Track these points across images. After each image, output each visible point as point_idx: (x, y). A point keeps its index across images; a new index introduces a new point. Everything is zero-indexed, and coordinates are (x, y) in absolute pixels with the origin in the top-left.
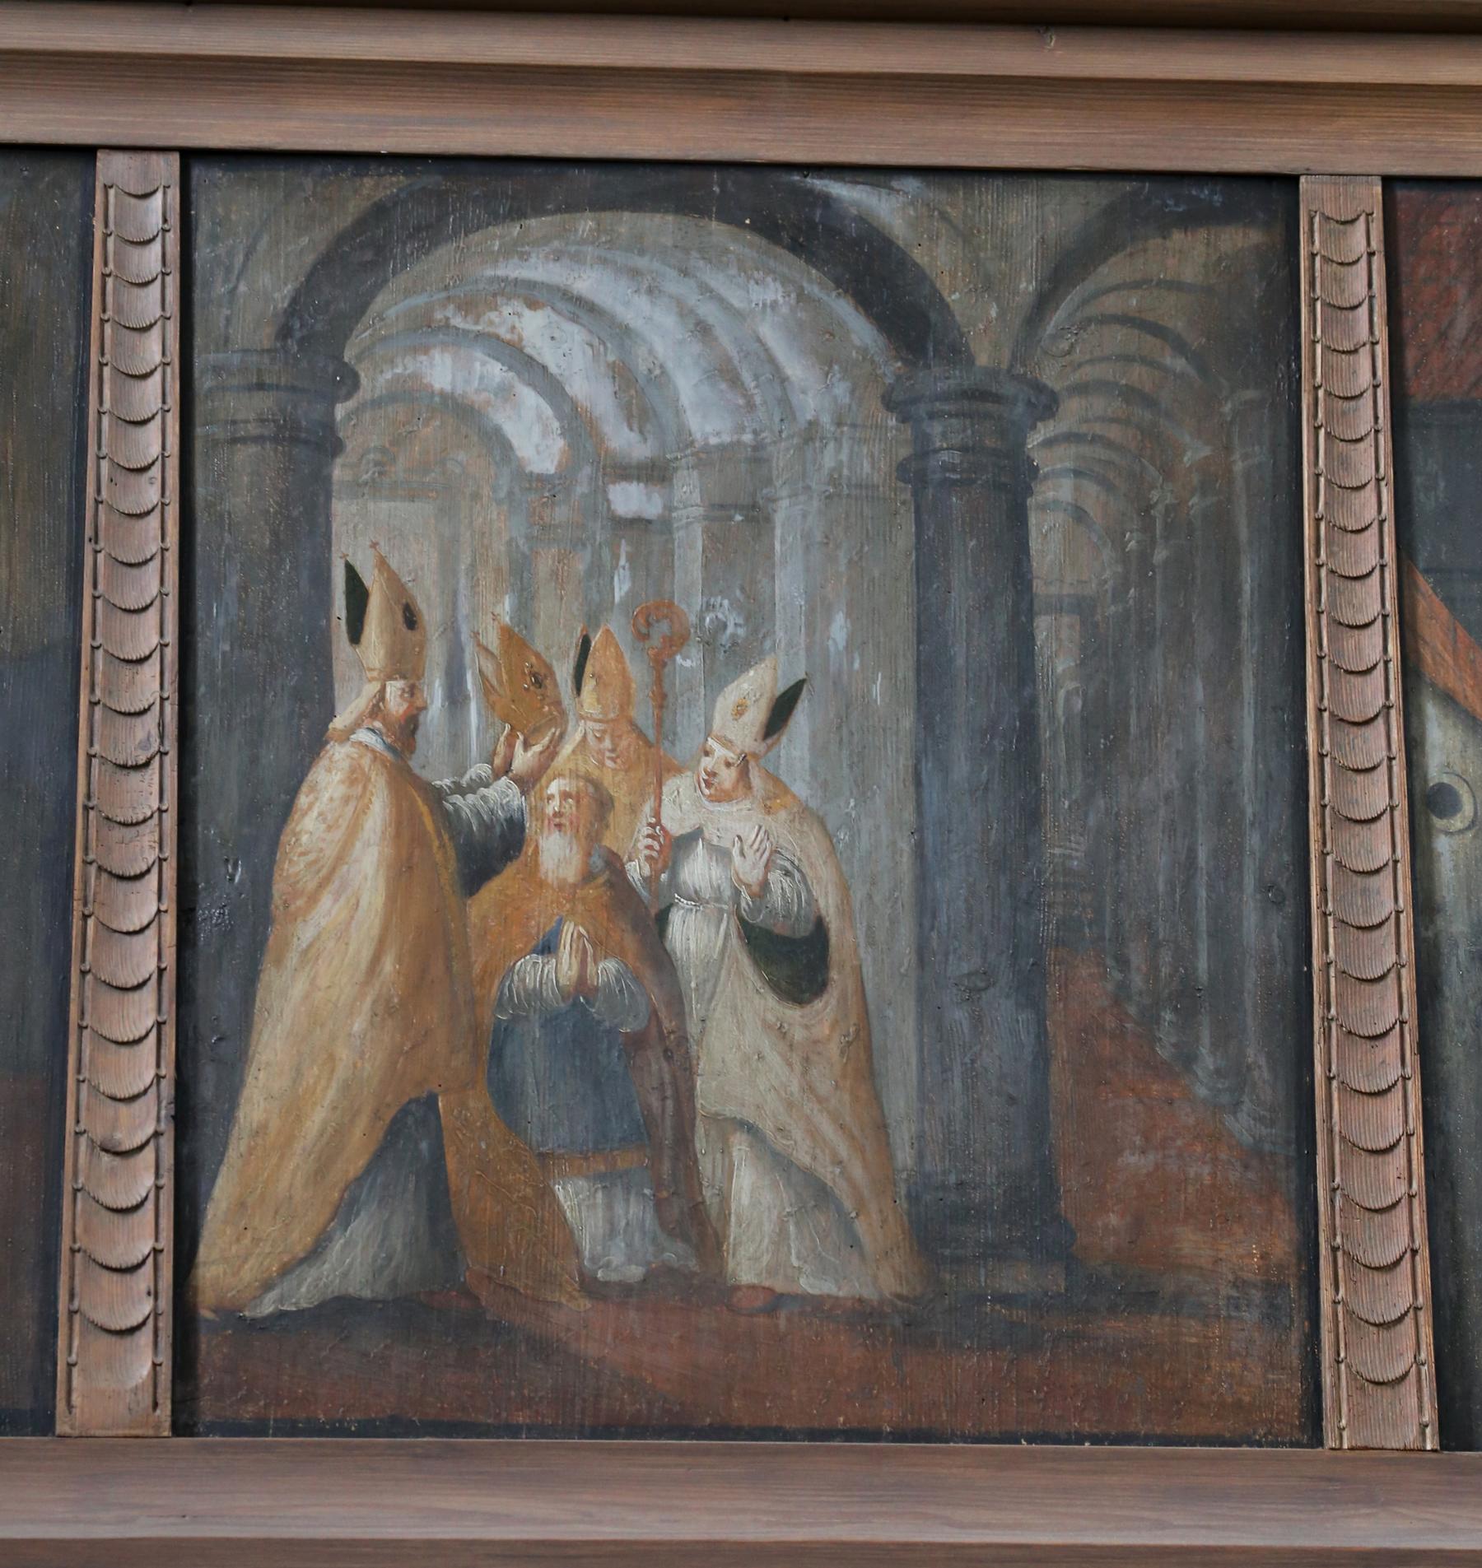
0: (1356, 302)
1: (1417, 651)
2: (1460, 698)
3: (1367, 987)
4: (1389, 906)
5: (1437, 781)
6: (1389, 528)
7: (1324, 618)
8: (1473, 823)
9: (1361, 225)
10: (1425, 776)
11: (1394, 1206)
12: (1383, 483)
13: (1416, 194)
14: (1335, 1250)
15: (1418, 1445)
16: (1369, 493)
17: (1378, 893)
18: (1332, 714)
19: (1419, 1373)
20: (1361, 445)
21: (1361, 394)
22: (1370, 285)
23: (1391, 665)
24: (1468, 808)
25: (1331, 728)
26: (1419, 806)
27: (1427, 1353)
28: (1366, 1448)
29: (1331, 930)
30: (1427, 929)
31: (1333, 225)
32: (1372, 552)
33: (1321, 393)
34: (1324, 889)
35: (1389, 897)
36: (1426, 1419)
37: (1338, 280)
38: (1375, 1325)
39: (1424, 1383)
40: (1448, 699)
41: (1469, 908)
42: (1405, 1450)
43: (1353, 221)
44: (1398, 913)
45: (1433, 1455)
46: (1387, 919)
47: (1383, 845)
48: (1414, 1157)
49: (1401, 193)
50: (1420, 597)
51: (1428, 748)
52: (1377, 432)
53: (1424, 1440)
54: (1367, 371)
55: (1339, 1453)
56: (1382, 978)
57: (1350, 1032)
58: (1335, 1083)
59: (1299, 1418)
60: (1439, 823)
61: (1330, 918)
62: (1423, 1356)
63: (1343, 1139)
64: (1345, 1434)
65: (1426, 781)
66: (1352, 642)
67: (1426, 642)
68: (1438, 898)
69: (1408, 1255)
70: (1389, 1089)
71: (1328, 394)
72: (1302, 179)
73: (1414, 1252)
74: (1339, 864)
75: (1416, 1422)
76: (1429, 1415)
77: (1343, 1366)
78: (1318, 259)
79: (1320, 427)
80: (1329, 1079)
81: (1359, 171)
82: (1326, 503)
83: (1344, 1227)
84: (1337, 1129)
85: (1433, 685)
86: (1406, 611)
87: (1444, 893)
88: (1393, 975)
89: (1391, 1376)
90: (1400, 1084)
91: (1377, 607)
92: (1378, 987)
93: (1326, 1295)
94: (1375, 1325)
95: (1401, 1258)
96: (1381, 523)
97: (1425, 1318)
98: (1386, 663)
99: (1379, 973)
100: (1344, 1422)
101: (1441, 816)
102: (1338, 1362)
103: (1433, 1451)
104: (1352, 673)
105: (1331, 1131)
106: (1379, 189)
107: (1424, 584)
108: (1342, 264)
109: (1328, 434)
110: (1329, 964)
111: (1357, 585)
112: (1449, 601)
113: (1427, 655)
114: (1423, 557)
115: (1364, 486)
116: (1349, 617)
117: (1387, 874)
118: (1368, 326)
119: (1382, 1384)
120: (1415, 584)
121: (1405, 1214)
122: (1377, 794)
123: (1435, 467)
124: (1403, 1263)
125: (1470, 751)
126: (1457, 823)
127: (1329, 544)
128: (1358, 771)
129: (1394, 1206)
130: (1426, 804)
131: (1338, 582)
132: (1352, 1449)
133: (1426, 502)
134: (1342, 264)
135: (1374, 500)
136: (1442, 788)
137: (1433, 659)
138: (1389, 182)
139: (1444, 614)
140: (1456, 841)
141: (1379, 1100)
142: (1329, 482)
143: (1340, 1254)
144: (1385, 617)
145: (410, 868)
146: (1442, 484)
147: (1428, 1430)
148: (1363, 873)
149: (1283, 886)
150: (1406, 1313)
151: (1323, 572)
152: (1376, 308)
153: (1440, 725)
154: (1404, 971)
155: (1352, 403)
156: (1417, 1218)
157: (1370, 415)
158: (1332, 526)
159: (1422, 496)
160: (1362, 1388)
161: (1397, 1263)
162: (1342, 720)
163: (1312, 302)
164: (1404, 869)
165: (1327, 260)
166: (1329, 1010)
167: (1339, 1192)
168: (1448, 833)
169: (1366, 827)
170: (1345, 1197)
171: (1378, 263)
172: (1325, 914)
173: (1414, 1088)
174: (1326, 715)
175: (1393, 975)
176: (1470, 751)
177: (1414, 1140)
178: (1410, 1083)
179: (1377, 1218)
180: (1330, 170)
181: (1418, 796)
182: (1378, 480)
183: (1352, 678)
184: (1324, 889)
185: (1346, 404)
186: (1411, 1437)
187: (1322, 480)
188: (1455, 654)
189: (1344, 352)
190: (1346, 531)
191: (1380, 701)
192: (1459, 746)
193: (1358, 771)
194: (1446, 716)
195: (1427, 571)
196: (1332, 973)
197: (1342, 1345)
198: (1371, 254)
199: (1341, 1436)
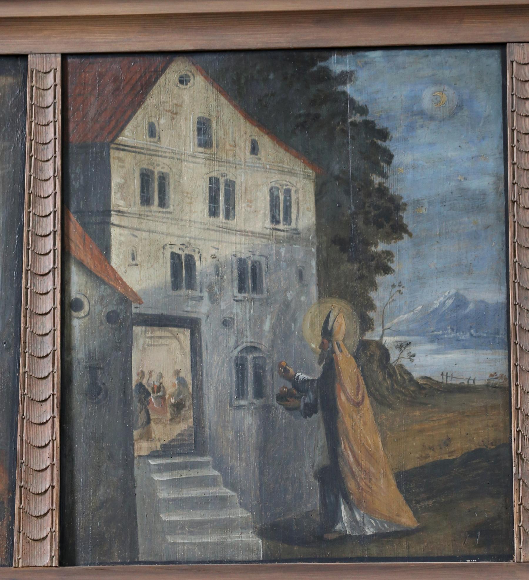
0: (49, 105)
1: (69, 245)
2: (85, 263)
3: (41, 381)
4: (51, 349)
5: (74, 297)
6: (59, 196)
7: (30, 233)
8: (88, 313)
9: (52, 73)
10: (70, 294)
11: (46, 469)
12: (57, 178)
13: (77, 60)
14: (21, 487)
15: (50, 564)
16: (51, 182)
17: (47, 343)
18: (32, 272)
19: (52, 536)
20: (49, 163)
21: (50, 142)
22: (55, 98)
23: (56, 251)
24: (86, 308)
25: (31, 277)
26: (67, 307)
27: (56, 528)
28: (35, 566)
29: (27, 359)
30: (67, 357)
31: (41, 74)
32: (49, 206)
33: (33, 142)
34: (25, 342)
35: (49, 345)
36: (53, 554)
37: (43, 96)
38: (35, 517)
39: (54, 540)
40: (81, 264)
41: (85, 349)
42: (44, 566)
43: (49, 72)
44: (54, 351)
45: (56, 569)
46: (50, 354)
47: (48, 324)
48: (55, 449)
49: (70, 60)
50: (71, 223)
51: (72, 284)
52: (55, 157)
53: (52, 563)
54: (51, 133)
55: (17, 569)
56: (47, 377)
57: (32, 399)
58: (25, 420)
59: (5, 555)
60: (75, 314)
61: (27, 354)
62: (54, 529)
63: (27, 442)
64: (20, 561)
65: (70, 297)
66: (42, 242)
67: (73, 241)
68: (73, 344)
69: (50, 489)
70: (47, 422)
71: (36, 142)
72: (29, 56)
73: (53, 487)
74: (31, 332)
75: (49, 555)
76: (55, 552)
77: (21, 534)
78: (34, 88)
79: (32, 156)
80: (23, 419)
81: (51, 52)
82: (33, 187)
83: (25, 478)
84: (24, 439)
85: (75, 258)
86: (65, 229)
87: (75, 342)
88: (51, 376)
89: (41, 537)
90: (51, 419)
91: (52, 228)
92: (44, 381)
93: (17, 506)
94: (35, 517)
95: (47, 490)
96: (55, 194)
97: (56, 514)
98: (55, 250)
99: (45, 375)
100: (20, 557)
101: (75, 311)
102: (19, 532)
103: (56, 567)
104: (41, 255)
105: (22, 439)
106: (59, 59)
107: (73, 218)
108: (44, 90)
109: (35, 159)
110: (25, 372)
111: (45, 219)
112: (84, 225)
113: (73, 246)
114: (73, 206)
115: (49, 179)
116: (40, 232)
117: (50, 336)
118: (52, 115)
119: (37, 540)
120: (69, 218)
121: (50, 472)
122: (47, 304)
123: (79, 171)
124: (48, 492)
125: (89, 285)
126: (82, 314)
127: (34, 204)
128: (41, 294)
129: (46, 469)
130: (67, 306)
131: (37, 218)
132: (22, 567)
133: (75, 184)
134: (44, 90)
135: (53, 185)
136: (77, 301)
137: (75, 248)
138: (65, 56)
139: (80, 229)
140: (81, 322)
141: (43, 426)
142: (34, 178)
143: (23, 489)
144: (55, 232)
145: (283, 171)
146: (82, 178)
147: (54, 559)
148: (41, 335)
149: (10, 341)
150: (48, 512)
151: (31, 214)
152: (57, 107)
153: (77, 274)
154: (55, 374)
155: (46, 146)
156: (55, 473)
157: (51, 152)
158: (35, 196)
159: (74, 183)
160: (29, 542)
161: (46, 491)
162: (36, 274)
163: (31, 105)
164: (58, 333)
165: (37, 88)
166: (24, 391)
167: (24, 464)
168: (77, 318)
169: (44, 317)
170: (26, 466)
171: (59, 89)
172: (25, 353)
173: (57, 421)
174: (29, 272)
175: (51, 376)
176: (89, 285)
177: (55, 442)
178: (55, 419)
179: (39, 474)
180: (40, 52)
181: (67, 302)
182: (55, 177)
183: (41, 257)
184: (25, 342)
185: (43, 146)
186: (46, 561)
187: (32, 177)
188: (84, 245)
189: (43, 125)
190: (41, 197)
191: (51, 266)
192: (84, 283)
193: (41, 294)
194: (80, 271)
195: (75, 213)
196: (26, 376)
197: (21, 525)
198: (56, 86)
199: (19, 562)
